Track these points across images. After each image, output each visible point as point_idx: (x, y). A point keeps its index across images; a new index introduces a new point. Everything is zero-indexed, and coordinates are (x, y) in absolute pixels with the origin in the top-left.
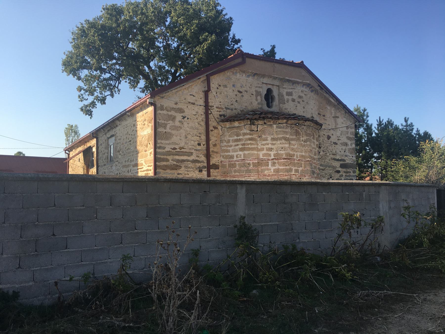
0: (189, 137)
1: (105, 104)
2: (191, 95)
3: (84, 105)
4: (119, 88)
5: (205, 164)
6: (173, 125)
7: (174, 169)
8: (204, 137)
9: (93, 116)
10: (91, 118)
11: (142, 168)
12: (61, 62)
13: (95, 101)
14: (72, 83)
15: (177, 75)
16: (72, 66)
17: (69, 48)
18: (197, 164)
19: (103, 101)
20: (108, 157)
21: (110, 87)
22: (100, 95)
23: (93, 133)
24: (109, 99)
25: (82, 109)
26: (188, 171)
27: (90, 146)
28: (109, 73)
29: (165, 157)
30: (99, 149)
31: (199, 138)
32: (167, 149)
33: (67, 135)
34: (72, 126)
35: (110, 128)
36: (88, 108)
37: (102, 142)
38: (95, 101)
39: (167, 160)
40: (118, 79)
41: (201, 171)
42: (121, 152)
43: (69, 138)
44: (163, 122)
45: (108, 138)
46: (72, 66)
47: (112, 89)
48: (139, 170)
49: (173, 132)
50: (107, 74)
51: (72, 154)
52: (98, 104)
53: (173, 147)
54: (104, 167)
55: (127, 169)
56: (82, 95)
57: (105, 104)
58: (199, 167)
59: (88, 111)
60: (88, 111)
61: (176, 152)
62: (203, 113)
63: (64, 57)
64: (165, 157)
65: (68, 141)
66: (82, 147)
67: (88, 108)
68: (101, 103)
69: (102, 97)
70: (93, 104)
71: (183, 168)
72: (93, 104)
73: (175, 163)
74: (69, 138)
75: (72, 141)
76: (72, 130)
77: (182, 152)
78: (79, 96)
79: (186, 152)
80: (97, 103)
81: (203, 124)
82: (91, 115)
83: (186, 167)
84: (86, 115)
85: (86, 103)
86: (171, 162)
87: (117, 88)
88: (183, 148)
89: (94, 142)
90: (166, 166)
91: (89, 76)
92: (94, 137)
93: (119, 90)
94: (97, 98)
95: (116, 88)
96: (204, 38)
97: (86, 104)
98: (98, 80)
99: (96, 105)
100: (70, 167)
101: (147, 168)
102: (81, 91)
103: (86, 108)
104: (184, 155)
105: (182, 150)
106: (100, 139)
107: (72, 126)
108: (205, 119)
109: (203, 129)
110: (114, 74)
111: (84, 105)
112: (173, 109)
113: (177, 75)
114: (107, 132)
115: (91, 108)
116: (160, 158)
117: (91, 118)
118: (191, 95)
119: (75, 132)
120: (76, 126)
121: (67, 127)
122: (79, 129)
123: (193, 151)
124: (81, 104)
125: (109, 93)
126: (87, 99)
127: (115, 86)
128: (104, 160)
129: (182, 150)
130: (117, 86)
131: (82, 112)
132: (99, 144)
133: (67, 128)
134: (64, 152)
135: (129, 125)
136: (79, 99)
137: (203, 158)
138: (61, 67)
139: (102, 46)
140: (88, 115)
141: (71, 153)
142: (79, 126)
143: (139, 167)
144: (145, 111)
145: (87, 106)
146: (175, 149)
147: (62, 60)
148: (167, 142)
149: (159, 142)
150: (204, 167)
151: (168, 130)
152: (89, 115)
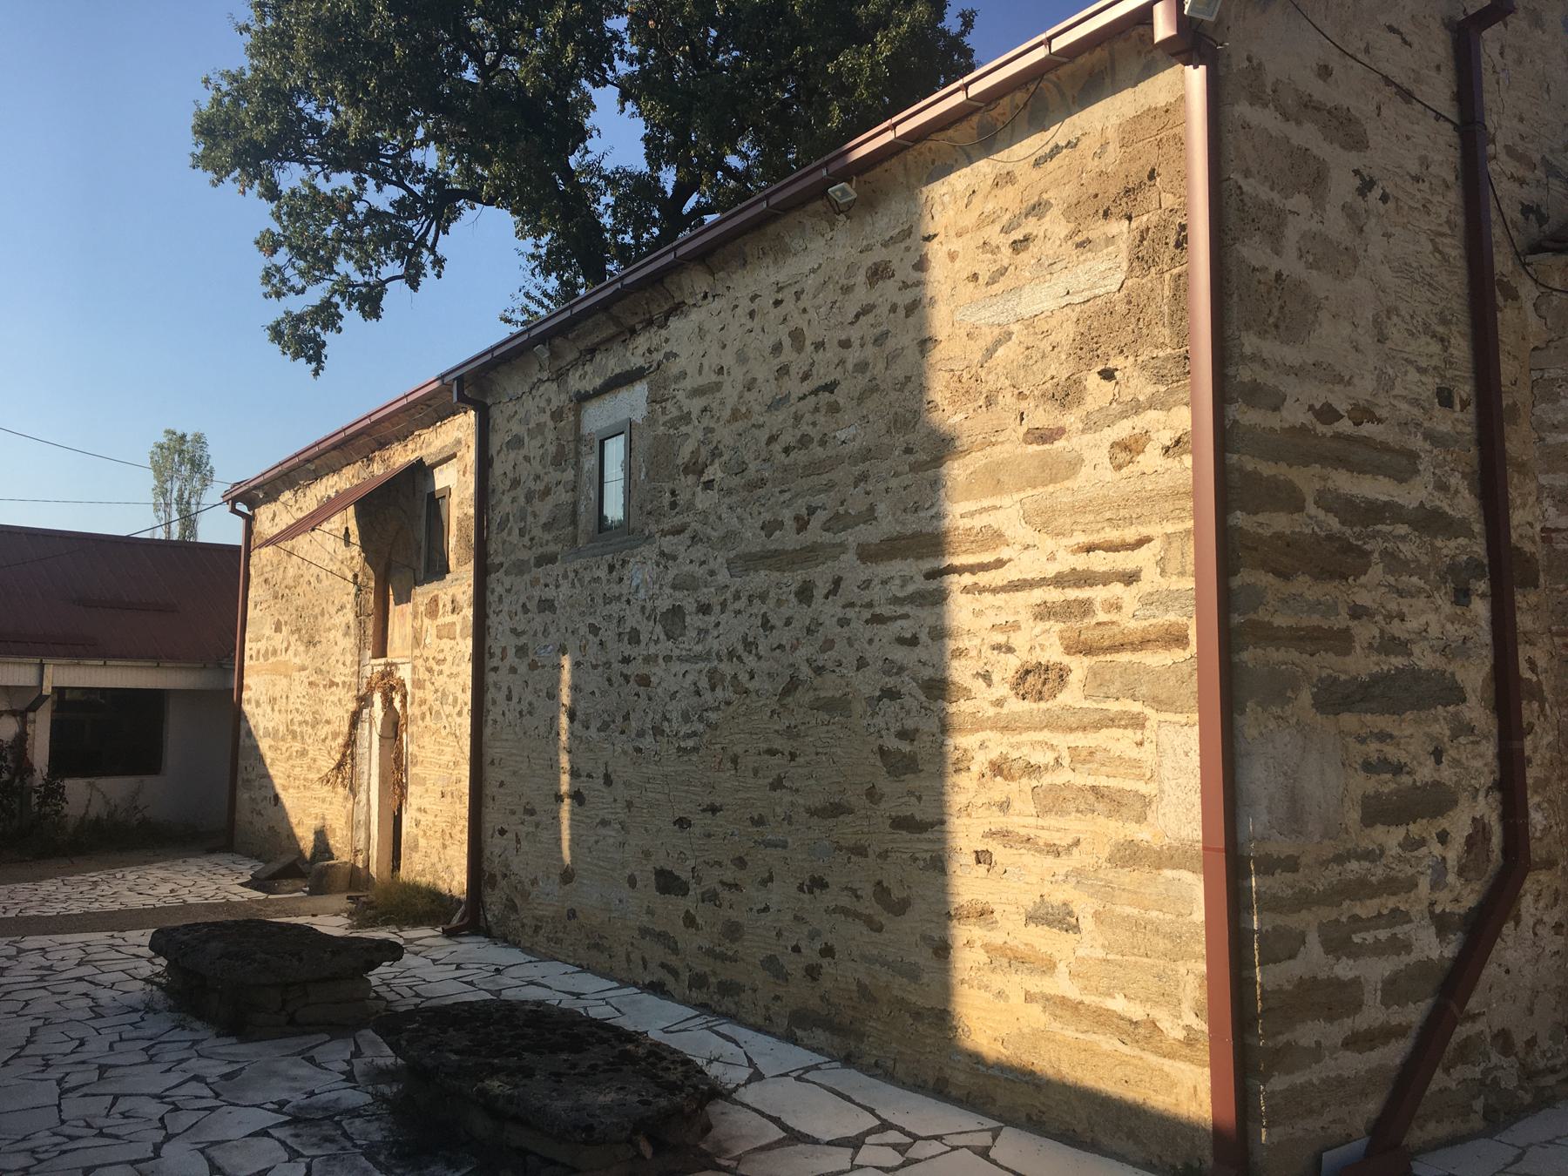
0: (1396, 333)
1: (378, 317)
2: (1391, 29)
3: (288, 313)
4: (440, 250)
5: (1479, 549)
6: (1314, 226)
7: (1331, 577)
8: (1461, 349)
9: (327, 364)
10: (316, 373)
11: (1000, 564)
12: (193, 121)
13: (337, 299)
14: (244, 212)
15: (687, 208)
16: (242, 139)
17: (236, 56)
18: (1439, 543)
19: (370, 302)
20: (575, 513)
21: (406, 242)
22: (357, 277)
23: (460, 379)
24: (396, 295)
25: (276, 333)
26: (1400, 593)
27: (420, 461)
28: (400, 184)
29: (1280, 471)
30: (498, 468)
31: (1435, 348)
32: (1295, 414)
33: (158, 470)
34: (184, 436)
35: (612, 330)
36: (305, 327)
37: (516, 428)
38: (337, 299)
39: (1292, 501)
40: (441, 205)
41: (1462, 596)
42: (714, 472)
43: (168, 485)
44: (1265, 193)
45: (583, 398)
46: (242, 139)
47: (411, 253)
48: (956, 582)
49: (1319, 283)
50: (388, 188)
51: (271, 519)
52: (351, 317)
53: (1320, 394)
54: (538, 572)
55: (800, 576)
56: (279, 269)
57: (378, 317)
58: (1453, 569)
59: (303, 340)
60: (303, 340)
61: (1337, 436)
62: (1451, 178)
63: (206, 99)
64: (1280, 471)
65: (164, 494)
66: (348, 472)
67: (305, 327)
68: (361, 308)
69: (366, 284)
70: (327, 315)
71: (1376, 572)
72: (327, 315)
73: (1334, 523)
74: (168, 485)
75: (181, 496)
76: (181, 452)
77: (1365, 441)
78: (268, 276)
79: (1385, 448)
80: (342, 309)
81: (1454, 249)
82: (319, 361)
83: (1394, 562)
84: (296, 356)
85: (297, 304)
86: (1319, 521)
87: (432, 250)
88: (1375, 419)
89: (461, 428)
90: (1289, 543)
91: (304, 198)
92: (465, 402)
93: (439, 262)
94: (345, 288)
95: (425, 253)
96: (874, 15)
97: (297, 311)
98: (344, 221)
99: (340, 317)
100: (254, 581)
101: (1081, 562)
102: (274, 251)
103: (296, 327)
104: (1377, 470)
105: (1368, 429)
106: (498, 417)
107: (184, 436)
108: (1460, 220)
109: (1455, 283)
110: (419, 189)
111: (288, 313)
112: (1309, 106)
113: (687, 208)
114: (574, 364)
115: (317, 329)
116: (1254, 477)
117: (316, 373)
118: (1391, 29)
119: (192, 461)
120: (199, 439)
121: (163, 440)
122: (210, 450)
123: (1418, 443)
124: (276, 310)
125: (394, 268)
126: (303, 291)
127: (421, 242)
128: (537, 532)
129: (1368, 429)
130: (429, 244)
131: (277, 348)
132: (496, 441)
133: (161, 447)
134: (228, 507)
135: (811, 283)
136: (268, 289)
137: (1465, 505)
138: (189, 144)
139: (400, 33)
140: (303, 360)
141: (264, 513)
142: (209, 439)
143: (957, 561)
144: (1059, 133)
145: (300, 319)
146: (1327, 414)
147: (195, 108)
148: (1291, 355)
149: (1248, 350)
150: (1474, 567)
151: (1290, 264)
152: (309, 361)
